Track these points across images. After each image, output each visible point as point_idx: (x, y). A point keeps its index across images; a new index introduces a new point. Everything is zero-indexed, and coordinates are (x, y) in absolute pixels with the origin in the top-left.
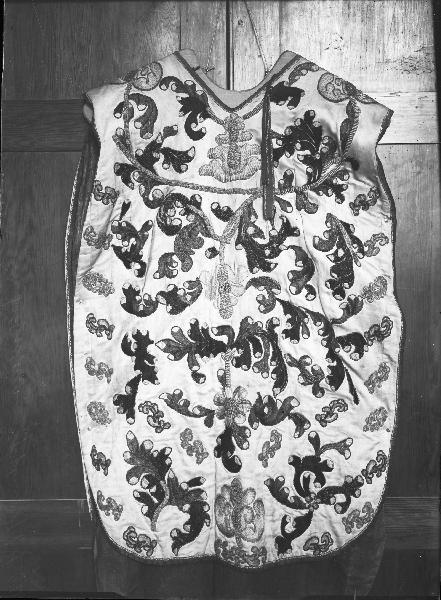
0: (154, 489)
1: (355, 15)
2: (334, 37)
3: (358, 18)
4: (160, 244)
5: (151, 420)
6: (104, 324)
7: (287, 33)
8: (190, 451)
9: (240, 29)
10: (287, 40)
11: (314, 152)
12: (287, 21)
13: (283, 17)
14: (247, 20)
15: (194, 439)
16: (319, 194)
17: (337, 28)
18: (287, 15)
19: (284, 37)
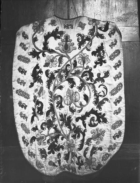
0: (66, 76)
1: (104, 5)
2: (99, 11)
3: (105, 6)
4: (42, 118)
5: (116, 134)
6: (27, 141)
7: (85, 11)
8: (21, 83)
9: (72, 10)
10: (85, 13)
11: (54, 142)
12: (85, 7)
13: (84, 6)
14: (73, 7)
15: (25, 139)
16: (60, 131)
17: (99, 9)
18: (85, 6)
19: (84, 12)
